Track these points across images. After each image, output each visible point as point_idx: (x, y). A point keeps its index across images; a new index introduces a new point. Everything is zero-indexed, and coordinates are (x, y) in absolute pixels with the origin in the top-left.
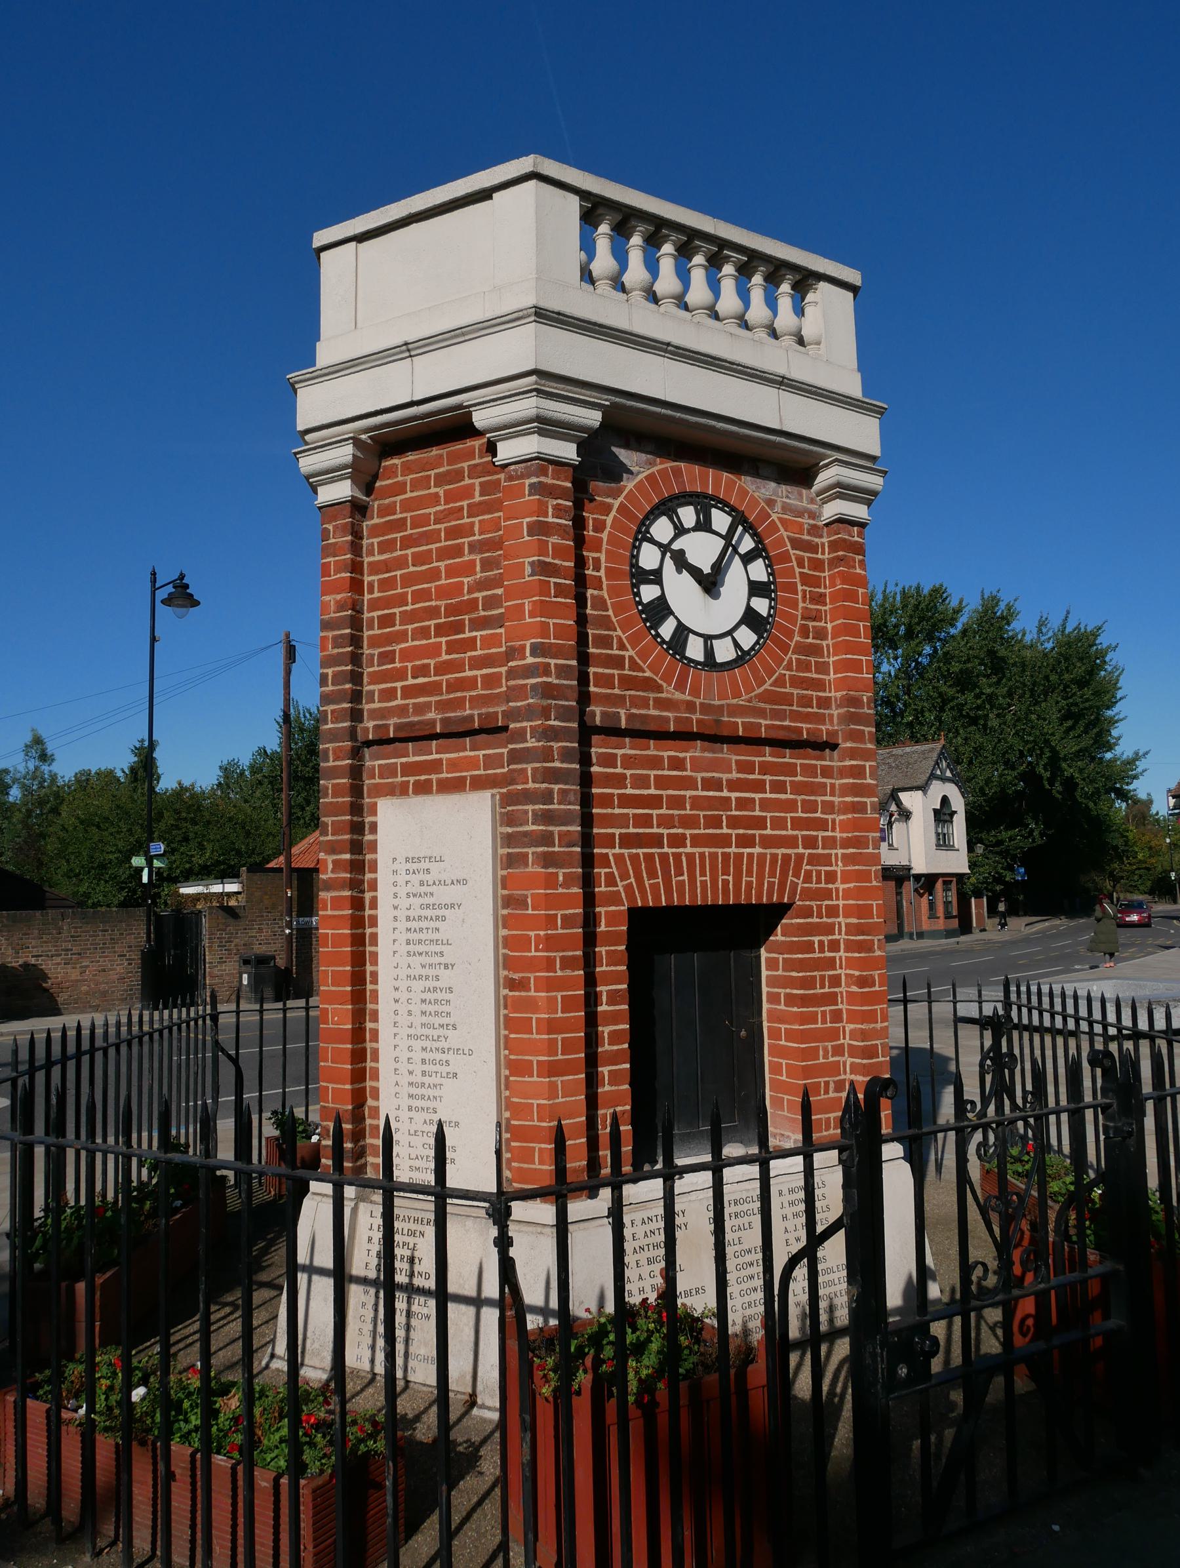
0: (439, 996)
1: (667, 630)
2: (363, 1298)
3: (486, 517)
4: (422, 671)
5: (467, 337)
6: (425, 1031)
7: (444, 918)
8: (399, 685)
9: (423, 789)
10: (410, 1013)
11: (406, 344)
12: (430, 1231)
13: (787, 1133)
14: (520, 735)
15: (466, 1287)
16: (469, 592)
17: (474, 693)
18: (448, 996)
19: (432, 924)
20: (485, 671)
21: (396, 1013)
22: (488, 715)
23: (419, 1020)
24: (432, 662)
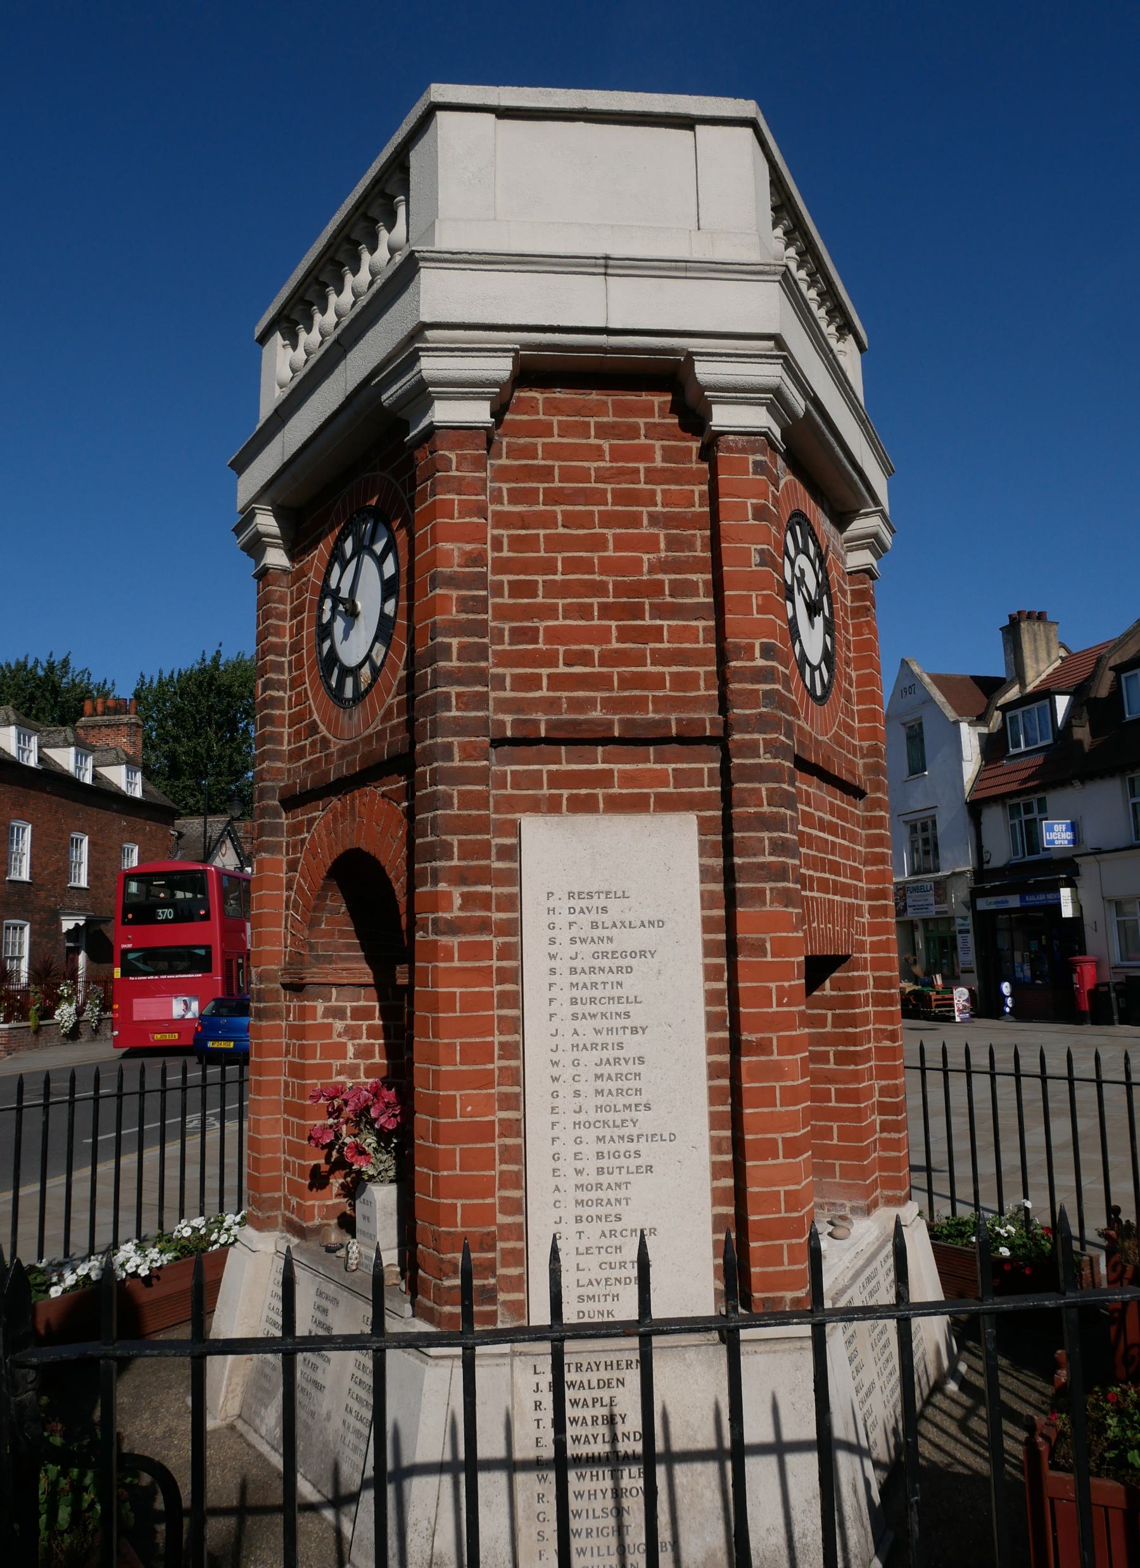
0: (623, 1068)
2: (538, 1488)
3: (673, 487)
5: (689, 274)
8: (545, 671)
10: (577, 1094)
11: (607, 258)
12: (633, 1377)
13: (839, 1202)
14: (773, 748)
15: (699, 1437)
16: (650, 572)
17: (660, 694)
18: (638, 1068)
19: (612, 978)
20: (674, 669)
21: (555, 1095)
22: (691, 721)
24: (597, 650)
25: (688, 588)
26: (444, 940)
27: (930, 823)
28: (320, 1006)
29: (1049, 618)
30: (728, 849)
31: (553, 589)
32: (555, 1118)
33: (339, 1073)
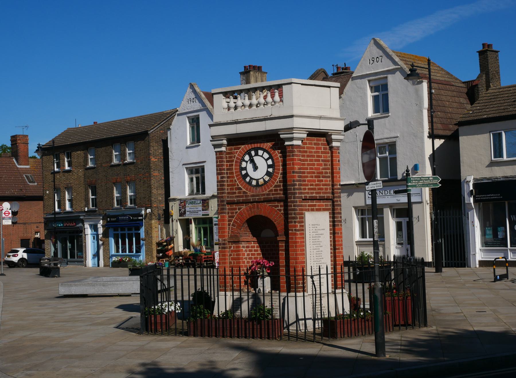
1: (248, 179)
4: (312, 185)
9: (312, 210)
25: (326, 173)
28: (241, 245)
29: (263, 70)
31: (308, 173)
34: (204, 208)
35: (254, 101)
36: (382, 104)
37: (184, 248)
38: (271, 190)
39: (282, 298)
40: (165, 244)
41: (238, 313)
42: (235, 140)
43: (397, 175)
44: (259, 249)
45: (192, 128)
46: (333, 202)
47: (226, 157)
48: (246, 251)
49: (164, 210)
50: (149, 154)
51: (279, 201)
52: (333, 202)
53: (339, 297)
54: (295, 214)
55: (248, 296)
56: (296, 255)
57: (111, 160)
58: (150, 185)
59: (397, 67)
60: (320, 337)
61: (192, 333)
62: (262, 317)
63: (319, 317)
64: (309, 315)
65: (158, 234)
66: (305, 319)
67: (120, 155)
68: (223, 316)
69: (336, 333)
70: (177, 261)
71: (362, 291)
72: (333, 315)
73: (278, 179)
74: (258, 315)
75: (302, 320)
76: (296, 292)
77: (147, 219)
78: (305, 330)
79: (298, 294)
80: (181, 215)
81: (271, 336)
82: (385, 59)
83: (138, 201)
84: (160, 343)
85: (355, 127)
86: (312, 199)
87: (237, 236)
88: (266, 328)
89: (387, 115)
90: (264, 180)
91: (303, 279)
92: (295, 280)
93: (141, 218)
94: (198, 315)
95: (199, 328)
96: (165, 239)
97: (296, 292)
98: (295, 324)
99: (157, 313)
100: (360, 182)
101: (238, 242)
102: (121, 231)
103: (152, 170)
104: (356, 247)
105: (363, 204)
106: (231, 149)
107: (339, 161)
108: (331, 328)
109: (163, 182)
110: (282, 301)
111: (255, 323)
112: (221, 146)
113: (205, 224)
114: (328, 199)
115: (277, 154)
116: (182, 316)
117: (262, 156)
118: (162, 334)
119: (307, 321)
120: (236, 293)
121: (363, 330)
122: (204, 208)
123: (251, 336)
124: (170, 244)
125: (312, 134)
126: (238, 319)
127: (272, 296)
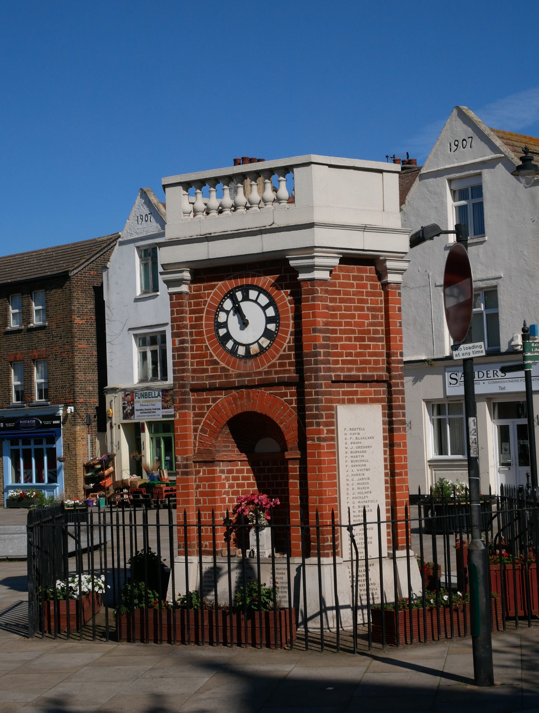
0: (364, 481)
1: (230, 345)
4: (350, 354)
6: (360, 495)
7: (365, 452)
8: (340, 359)
9: (351, 401)
10: (353, 489)
16: (367, 326)
18: (368, 481)
19: (361, 454)
21: (348, 489)
23: (357, 491)
24: (353, 352)
25: (376, 332)
26: (322, 443)
27: (159, 337)
28: (218, 469)
30: (390, 415)
32: (348, 496)
33: (224, 494)
34: (165, 405)
35: (241, 199)
36: (473, 221)
37: (131, 474)
38: (274, 365)
39: (293, 568)
40: (99, 466)
41: (211, 597)
42: (206, 273)
43: (499, 345)
44: (252, 475)
45: (145, 266)
46: (389, 386)
47: (190, 304)
48: (227, 479)
49: (97, 408)
50: (71, 311)
51: (287, 384)
52: (389, 386)
53: (402, 565)
54: (317, 408)
55: (229, 563)
56: (321, 485)
57: (6, 323)
58: (73, 366)
59: (498, 155)
60: (367, 643)
61: (124, 636)
62: (255, 605)
63: (365, 603)
64: (345, 599)
65: (87, 449)
66: (337, 608)
67: (22, 313)
68: (182, 602)
69: (397, 636)
70: (118, 497)
71: (444, 549)
72: (391, 598)
73: (286, 344)
74: (248, 601)
75: (331, 608)
76: (319, 556)
77: (68, 424)
78: (338, 628)
79: (324, 560)
80: (126, 416)
81: (273, 642)
82: (477, 142)
83: (52, 393)
84: (61, 655)
85: (431, 238)
86: (350, 381)
87: (210, 452)
88: (264, 625)
89: (481, 239)
90: (260, 346)
91: (334, 532)
92: (318, 533)
93: (58, 422)
94: (136, 601)
95: (138, 626)
96: (99, 457)
97: (319, 556)
98: (319, 617)
99: (61, 597)
100: (436, 357)
101: (212, 462)
102: (24, 444)
103: (76, 339)
104: (429, 470)
105: (441, 396)
106: (199, 289)
107: (400, 309)
108: (386, 624)
109: (95, 360)
110: (293, 574)
111: (242, 616)
112: (179, 282)
113: (163, 429)
114: (379, 381)
115: (285, 297)
116: (110, 599)
117: (256, 301)
118: (68, 637)
119: (342, 611)
120: (208, 559)
121: (448, 628)
122: (165, 405)
123: (235, 641)
124: (107, 468)
125: (350, 259)
126: (211, 608)
127: (273, 564)
